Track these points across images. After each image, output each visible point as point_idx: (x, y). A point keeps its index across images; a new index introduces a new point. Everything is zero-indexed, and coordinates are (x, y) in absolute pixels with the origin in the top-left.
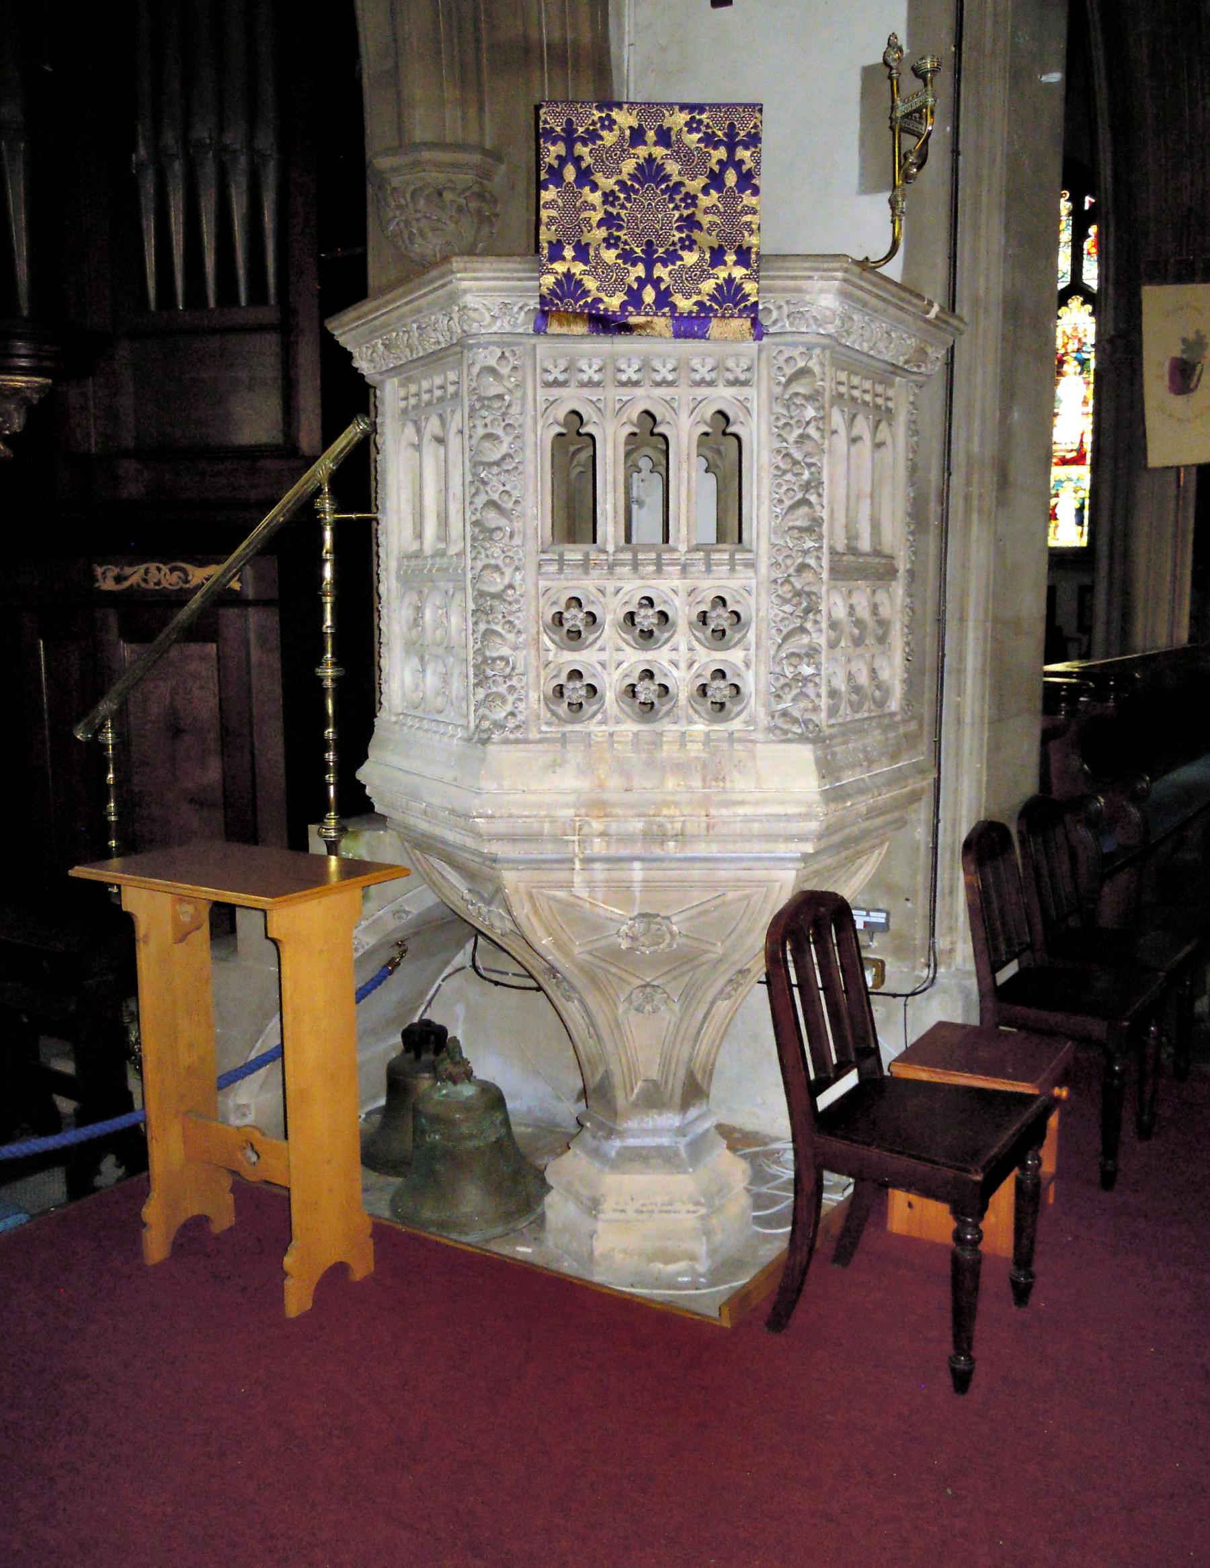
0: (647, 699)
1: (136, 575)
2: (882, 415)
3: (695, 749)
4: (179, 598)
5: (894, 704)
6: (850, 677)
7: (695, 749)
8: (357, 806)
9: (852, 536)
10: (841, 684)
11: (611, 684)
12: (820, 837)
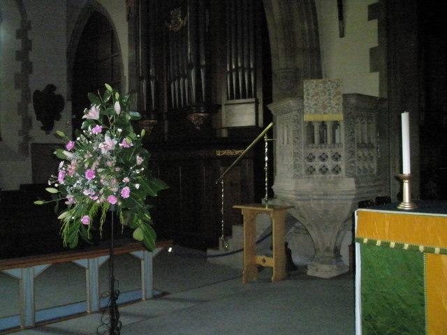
0: (324, 171)
1: (224, 152)
2: (369, 117)
3: (332, 179)
4: (235, 157)
5: (375, 172)
6: (363, 167)
7: (332, 179)
8: (272, 195)
9: (362, 139)
10: (361, 167)
11: (317, 168)
12: (355, 195)
